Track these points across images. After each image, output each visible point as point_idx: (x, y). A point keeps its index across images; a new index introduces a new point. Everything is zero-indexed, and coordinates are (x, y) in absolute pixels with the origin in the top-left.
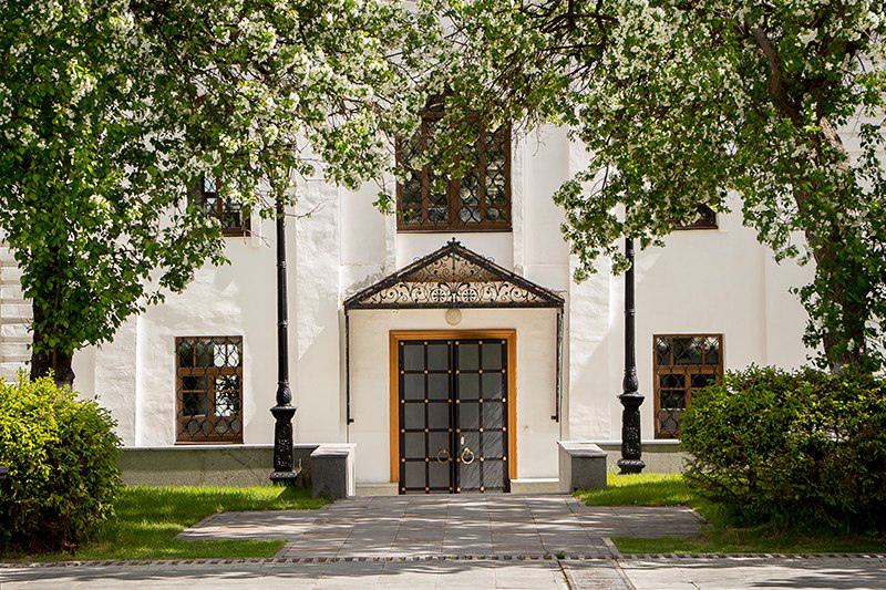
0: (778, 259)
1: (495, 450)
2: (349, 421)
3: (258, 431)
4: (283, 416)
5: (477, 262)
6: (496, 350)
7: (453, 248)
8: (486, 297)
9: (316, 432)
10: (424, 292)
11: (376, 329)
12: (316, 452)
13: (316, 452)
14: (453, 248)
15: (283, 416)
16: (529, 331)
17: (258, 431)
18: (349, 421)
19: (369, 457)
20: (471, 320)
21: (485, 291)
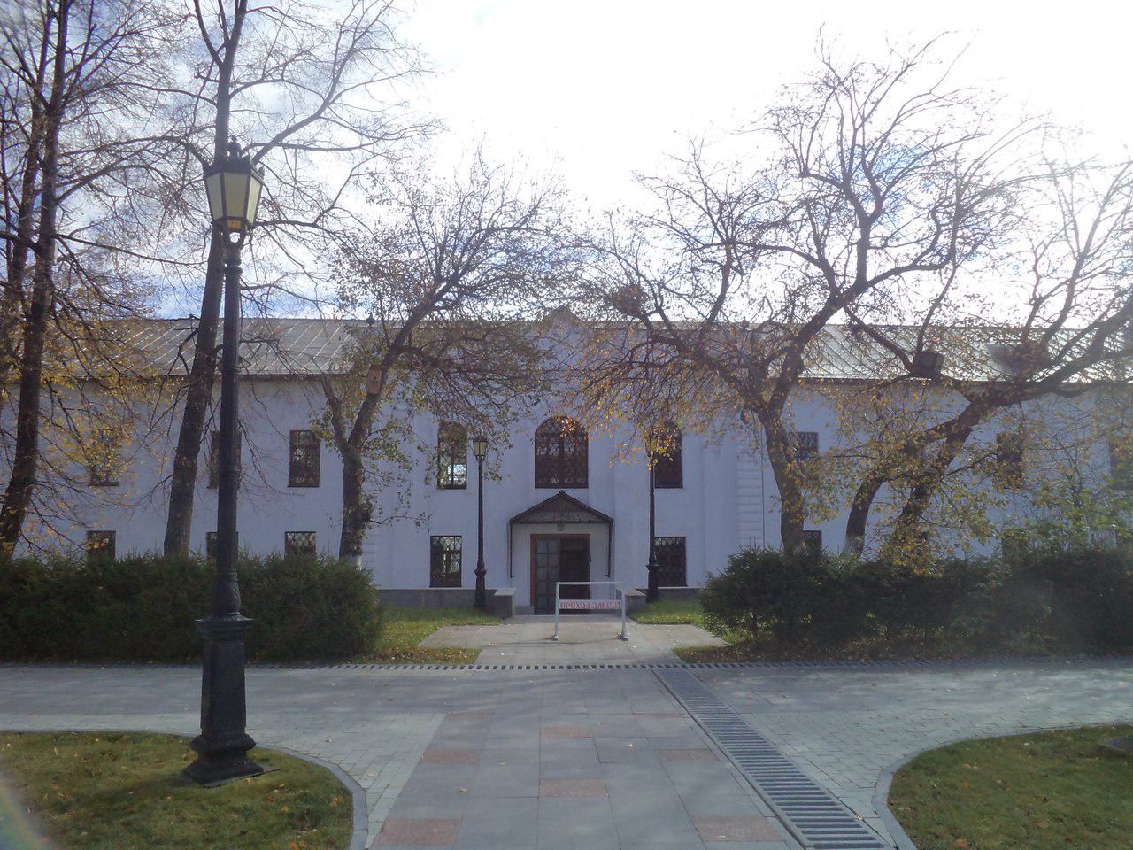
0: (510, 446)
1: (541, 560)
2: (511, 576)
3: (468, 582)
4: (480, 572)
5: (596, 515)
6: (584, 541)
7: (562, 496)
8: (577, 519)
9: (497, 584)
10: (548, 517)
11: (524, 536)
12: (497, 594)
13: (497, 594)
14: (562, 496)
15: (480, 572)
16: (596, 534)
17: (468, 582)
18: (511, 576)
19: (517, 589)
20: (570, 530)
21: (576, 516)
